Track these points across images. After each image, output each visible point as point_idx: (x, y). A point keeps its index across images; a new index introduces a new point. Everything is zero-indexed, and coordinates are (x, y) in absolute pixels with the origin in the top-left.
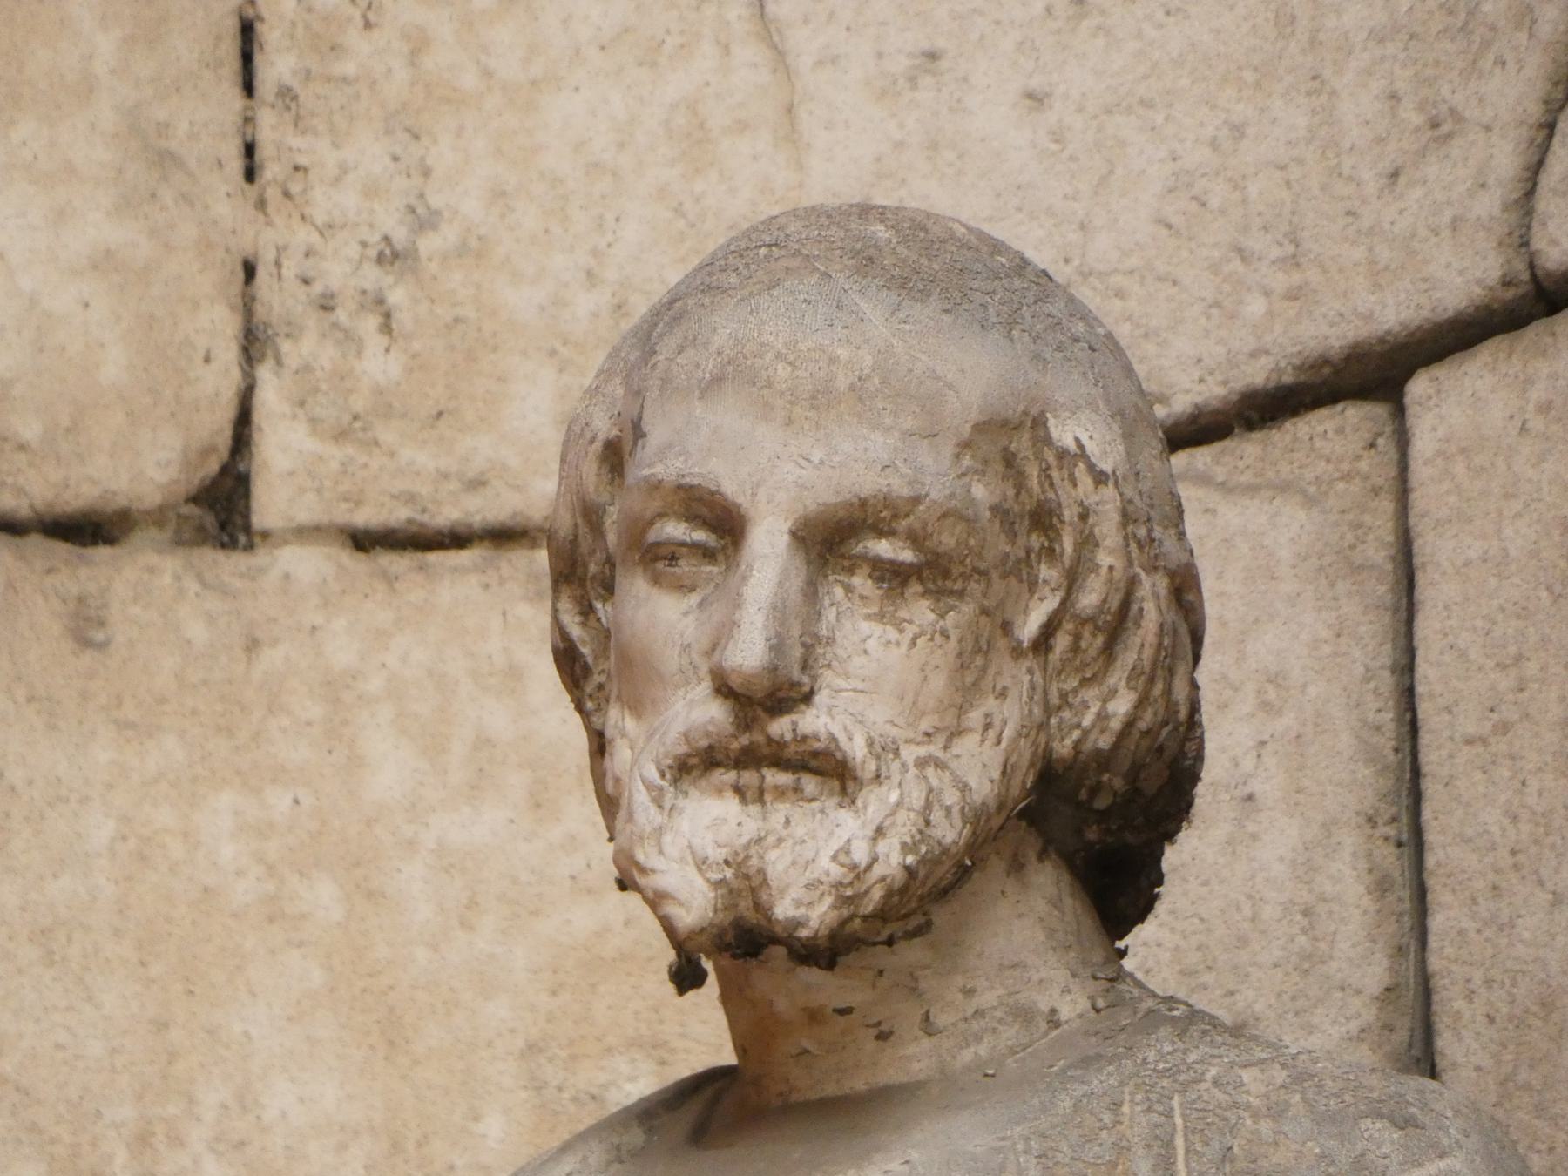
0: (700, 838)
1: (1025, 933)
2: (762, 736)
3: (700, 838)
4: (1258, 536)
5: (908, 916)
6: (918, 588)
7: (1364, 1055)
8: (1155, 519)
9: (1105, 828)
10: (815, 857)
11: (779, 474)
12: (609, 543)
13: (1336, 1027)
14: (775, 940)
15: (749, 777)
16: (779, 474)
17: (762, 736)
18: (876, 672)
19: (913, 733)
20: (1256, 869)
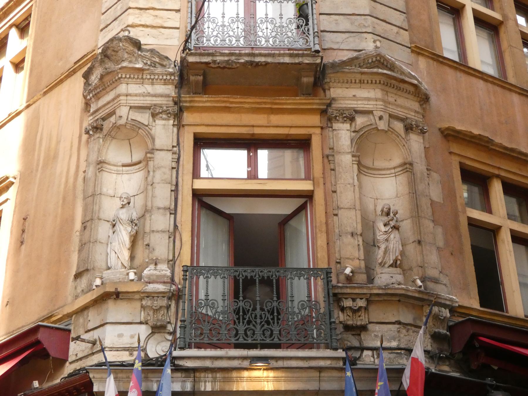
0: (122, 203)
1: (127, 205)
2: (123, 201)
3: (122, 203)
4: (132, 199)
5: (125, 204)
6: (447, 363)
7: (103, 159)
8: (319, 56)
9: (129, 203)
10: (124, 203)
11: (124, 197)
12: (121, 198)
13: (133, 207)
14: (303, 5)
15: (387, 88)
16: (124, 197)
17: (123, 201)
18: (125, 200)
19: (126, 201)
20: (131, 204)
